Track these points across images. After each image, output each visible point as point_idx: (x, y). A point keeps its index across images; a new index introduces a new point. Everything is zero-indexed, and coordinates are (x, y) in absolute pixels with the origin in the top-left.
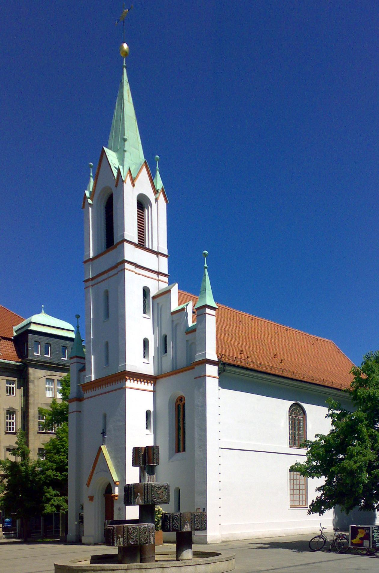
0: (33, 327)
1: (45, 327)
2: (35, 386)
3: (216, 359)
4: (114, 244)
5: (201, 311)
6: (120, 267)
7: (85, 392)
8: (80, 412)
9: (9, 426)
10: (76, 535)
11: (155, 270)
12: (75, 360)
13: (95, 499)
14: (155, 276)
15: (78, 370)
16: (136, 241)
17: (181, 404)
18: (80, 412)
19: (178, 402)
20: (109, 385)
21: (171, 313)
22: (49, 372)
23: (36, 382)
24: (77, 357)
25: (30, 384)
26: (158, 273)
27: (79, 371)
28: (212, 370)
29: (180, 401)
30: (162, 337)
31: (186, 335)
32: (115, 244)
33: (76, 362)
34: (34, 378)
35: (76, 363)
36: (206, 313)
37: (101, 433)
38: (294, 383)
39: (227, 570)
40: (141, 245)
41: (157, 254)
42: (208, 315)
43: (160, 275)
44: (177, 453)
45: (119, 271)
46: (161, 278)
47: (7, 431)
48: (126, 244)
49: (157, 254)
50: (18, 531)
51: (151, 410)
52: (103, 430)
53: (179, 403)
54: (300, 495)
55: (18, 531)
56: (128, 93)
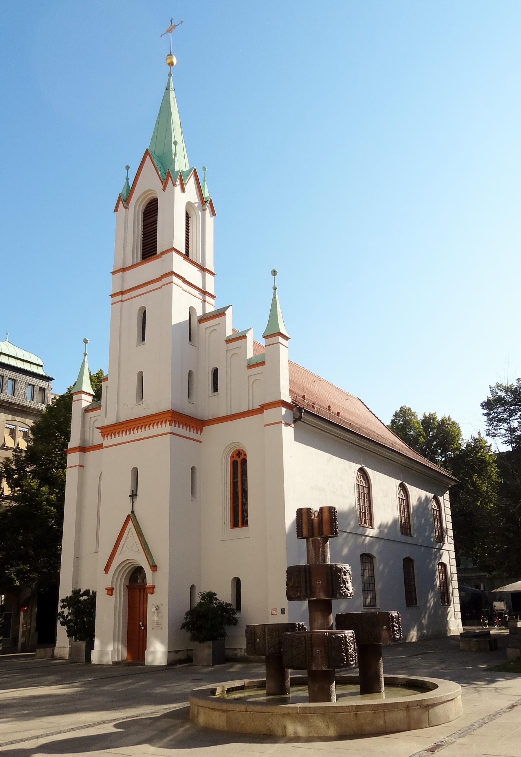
3: (289, 400)
4: (157, 254)
6: (165, 280)
7: (106, 437)
8: (83, 467)
11: (4, 356)
16: (184, 252)
17: (239, 460)
18: (83, 467)
19: (233, 457)
22: (10, 417)
29: (238, 457)
31: (248, 369)
37: (129, 496)
38: (347, 436)
39: (336, 715)
40: (186, 256)
42: (281, 345)
43: (207, 295)
44: (233, 528)
45: (163, 285)
51: (400, 483)
52: (133, 491)
54: (369, 583)
55: (11, 637)
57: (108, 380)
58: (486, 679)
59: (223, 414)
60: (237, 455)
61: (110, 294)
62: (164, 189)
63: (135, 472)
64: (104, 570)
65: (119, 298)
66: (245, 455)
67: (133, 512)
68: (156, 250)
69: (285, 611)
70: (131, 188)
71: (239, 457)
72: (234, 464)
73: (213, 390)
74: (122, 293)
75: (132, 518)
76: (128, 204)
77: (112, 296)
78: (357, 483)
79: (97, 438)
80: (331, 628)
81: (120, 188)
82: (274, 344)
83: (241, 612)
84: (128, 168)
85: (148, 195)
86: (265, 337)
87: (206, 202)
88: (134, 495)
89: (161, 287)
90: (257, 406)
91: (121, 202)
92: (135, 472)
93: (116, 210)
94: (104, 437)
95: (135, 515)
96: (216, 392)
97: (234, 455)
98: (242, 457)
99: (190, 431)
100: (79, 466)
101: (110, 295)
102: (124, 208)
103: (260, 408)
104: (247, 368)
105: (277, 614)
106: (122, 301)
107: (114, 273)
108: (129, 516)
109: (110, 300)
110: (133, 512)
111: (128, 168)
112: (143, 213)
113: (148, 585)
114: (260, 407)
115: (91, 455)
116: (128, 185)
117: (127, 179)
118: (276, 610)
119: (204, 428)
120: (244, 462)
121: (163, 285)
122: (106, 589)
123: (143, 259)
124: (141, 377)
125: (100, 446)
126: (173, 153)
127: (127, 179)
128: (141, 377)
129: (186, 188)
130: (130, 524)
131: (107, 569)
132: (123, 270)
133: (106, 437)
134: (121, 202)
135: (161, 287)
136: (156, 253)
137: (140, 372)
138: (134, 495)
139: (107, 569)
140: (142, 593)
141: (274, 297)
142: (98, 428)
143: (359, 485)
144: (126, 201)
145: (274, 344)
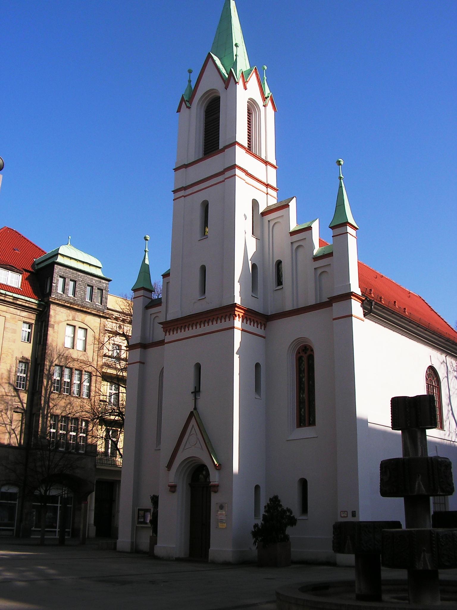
0: (60, 259)
1: (72, 260)
2: (54, 332)
4: (220, 148)
5: (339, 231)
6: (228, 174)
7: (168, 333)
9: (22, 382)
10: (132, 543)
12: (141, 293)
13: (179, 489)
14: (264, 188)
15: (144, 306)
16: (246, 145)
19: (299, 353)
20: (194, 327)
21: (290, 233)
23: (56, 326)
24: (144, 289)
25: (49, 328)
26: (267, 186)
27: (145, 307)
28: (357, 308)
30: (274, 264)
32: (221, 147)
33: (143, 296)
34: (55, 322)
35: (142, 297)
36: (348, 232)
37: (192, 393)
40: (249, 149)
41: (266, 163)
46: (270, 191)
47: (17, 388)
48: (237, 147)
49: (266, 163)
50: (138, 525)
53: (301, 354)
56: (234, 9)
57: (169, 276)
58: (45, 406)
59: (289, 307)
60: (303, 351)
61: (173, 168)
62: (226, 88)
63: (198, 367)
64: (167, 467)
65: (182, 193)
66: (312, 350)
67: (195, 409)
68: (219, 145)
69: (355, 513)
70: (193, 89)
71: (306, 353)
72: (299, 360)
73: (277, 285)
74: (185, 188)
75: (195, 415)
76: (191, 104)
77: (175, 192)
78: (427, 383)
79: (159, 334)
80: (111, 429)
81: (182, 90)
82: (342, 234)
83: (308, 515)
84: (190, 72)
85: (210, 94)
86: (332, 228)
87: (266, 98)
88: (197, 392)
89: (224, 181)
90: (325, 299)
91: (184, 103)
92: (198, 367)
93: (179, 111)
94: (166, 333)
95: (197, 412)
96: (280, 285)
97: (300, 351)
98: (309, 353)
99: (254, 326)
100: (140, 362)
101: (172, 191)
102: (187, 108)
103: (328, 301)
104: (313, 260)
105: (347, 517)
106: (185, 196)
107: (176, 170)
108: (192, 413)
109: (172, 196)
110: (195, 409)
111: (190, 72)
112: (205, 111)
113: (211, 483)
114: (328, 300)
115: (153, 352)
116: (191, 87)
117: (190, 81)
118: (346, 512)
119: (268, 323)
120: (311, 358)
121: (225, 179)
122: (169, 486)
123: (205, 154)
124: (203, 269)
125: (162, 343)
126: (235, 54)
127: (190, 81)
128: (203, 269)
129: (248, 85)
130: (193, 422)
131: (169, 466)
132: (186, 166)
133: (168, 333)
134: (184, 103)
135: (224, 181)
136: (219, 148)
137: (203, 265)
138: (197, 392)
139: (169, 466)
140: (7, 297)
141: (341, 187)
142: (160, 323)
143: (428, 384)
144: (188, 101)
145: (342, 234)
